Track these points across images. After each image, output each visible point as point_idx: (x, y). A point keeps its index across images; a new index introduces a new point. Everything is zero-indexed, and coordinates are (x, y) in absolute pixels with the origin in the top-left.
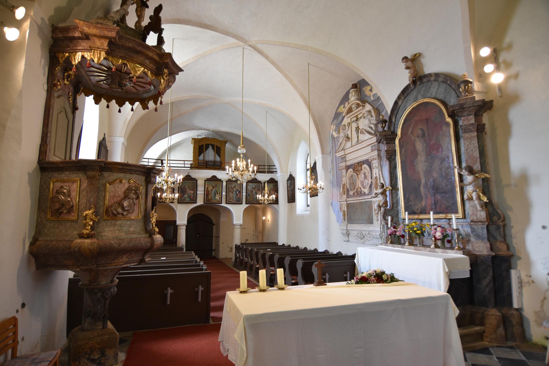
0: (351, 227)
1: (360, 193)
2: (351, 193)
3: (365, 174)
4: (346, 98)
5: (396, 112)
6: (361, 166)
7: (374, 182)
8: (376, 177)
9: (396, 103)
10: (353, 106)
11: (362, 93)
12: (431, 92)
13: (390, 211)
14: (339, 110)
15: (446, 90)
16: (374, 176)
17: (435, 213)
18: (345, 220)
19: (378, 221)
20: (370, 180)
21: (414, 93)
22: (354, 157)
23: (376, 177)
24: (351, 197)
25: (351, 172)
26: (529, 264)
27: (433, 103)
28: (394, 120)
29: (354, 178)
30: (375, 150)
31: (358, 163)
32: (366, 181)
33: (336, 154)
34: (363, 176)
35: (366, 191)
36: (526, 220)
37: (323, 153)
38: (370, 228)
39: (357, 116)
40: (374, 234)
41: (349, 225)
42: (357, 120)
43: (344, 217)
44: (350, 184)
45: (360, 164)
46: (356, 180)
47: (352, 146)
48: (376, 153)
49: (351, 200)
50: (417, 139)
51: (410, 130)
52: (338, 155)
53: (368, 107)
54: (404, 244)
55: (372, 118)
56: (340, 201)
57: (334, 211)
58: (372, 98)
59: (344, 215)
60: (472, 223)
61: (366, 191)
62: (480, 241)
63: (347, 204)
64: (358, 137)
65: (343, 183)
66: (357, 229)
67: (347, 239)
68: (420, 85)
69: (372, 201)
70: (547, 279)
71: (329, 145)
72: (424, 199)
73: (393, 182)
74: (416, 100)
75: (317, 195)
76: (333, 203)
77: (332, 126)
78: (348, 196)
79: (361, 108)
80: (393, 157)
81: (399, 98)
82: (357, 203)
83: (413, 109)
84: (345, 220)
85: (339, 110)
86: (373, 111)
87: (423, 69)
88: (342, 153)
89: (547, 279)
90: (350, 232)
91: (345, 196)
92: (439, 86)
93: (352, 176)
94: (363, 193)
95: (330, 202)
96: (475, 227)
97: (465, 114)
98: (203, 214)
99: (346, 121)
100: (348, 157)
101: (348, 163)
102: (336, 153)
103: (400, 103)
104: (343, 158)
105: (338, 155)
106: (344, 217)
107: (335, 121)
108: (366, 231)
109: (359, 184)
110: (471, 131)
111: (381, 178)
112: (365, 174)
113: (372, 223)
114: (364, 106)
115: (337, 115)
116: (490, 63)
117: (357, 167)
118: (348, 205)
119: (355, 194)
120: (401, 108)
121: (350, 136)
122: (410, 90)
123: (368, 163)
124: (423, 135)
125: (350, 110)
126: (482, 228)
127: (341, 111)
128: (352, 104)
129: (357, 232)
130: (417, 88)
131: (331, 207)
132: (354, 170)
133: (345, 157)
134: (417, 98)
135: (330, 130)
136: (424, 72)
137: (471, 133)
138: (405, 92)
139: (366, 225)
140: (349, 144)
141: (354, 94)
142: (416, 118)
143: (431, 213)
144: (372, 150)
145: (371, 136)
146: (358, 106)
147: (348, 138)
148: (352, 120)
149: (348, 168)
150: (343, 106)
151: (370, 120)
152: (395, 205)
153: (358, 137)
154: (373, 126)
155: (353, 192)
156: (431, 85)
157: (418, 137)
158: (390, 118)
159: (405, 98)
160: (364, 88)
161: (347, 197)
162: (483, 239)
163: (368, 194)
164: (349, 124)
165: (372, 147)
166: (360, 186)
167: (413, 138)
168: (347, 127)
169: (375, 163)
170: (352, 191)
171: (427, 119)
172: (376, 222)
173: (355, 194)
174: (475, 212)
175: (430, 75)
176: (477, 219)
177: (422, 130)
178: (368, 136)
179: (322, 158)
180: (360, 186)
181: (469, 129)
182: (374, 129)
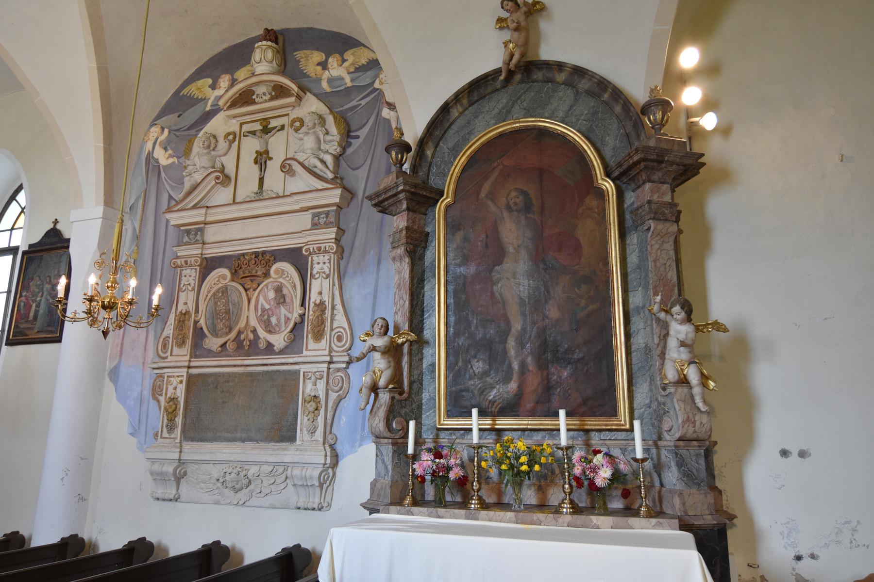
0: (194, 451)
1: (248, 346)
2: (213, 343)
3: (279, 290)
4: (236, 57)
5: (438, 133)
6: (268, 265)
7: (311, 315)
8: (322, 303)
9: (445, 109)
10: (260, 90)
11: (290, 65)
12: (552, 107)
13: (402, 401)
14: (193, 90)
15: (595, 113)
16: (314, 297)
17: (482, 414)
18: (171, 428)
19: (313, 432)
20: (298, 310)
21: (502, 99)
22: (236, 233)
23: (322, 303)
24: (210, 353)
25: (224, 277)
26: (753, 537)
27: (562, 137)
28: (429, 153)
29: (234, 297)
30: (327, 225)
31: (257, 255)
32: (283, 311)
33: (168, 216)
34: (271, 295)
35: (279, 340)
36: (747, 439)
37: (109, 201)
38: (287, 454)
39: (265, 122)
40: (297, 472)
41: (187, 446)
42: (266, 130)
43: (171, 420)
44: (214, 315)
45: (265, 259)
46: (240, 308)
47: (234, 202)
48: (331, 233)
49: (208, 366)
50: (506, 214)
51: (486, 187)
52: (175, 218)
53: (312, 105)
54: (557, 511)
55: (328, 138)
56: (154, 363)
57: (122, 399)
58: (325, 85)
59: (171, 414)
60: (681, 443)
61: (279, 340)
62: (694, 490)
63: (190, 377)
64: (261, 180)
65: (181, 308)
66: (224, 457)
67: (171, 492)
68: (522, 82)
69: (297, 372)
70: (794, 569)
71: (137, 185)
72: (515, 377)
73: (416, 321)
74: (504, 116)
75: (59, 340)
76: (123, 370)
77: (155, 130)
78: (198, 350)
79: (292, 99)
80: (419, 251)
81: (457, 97)
82: (234, 375)
83: (501, 135)
84: (171, 428)
85: (193, 90)
86: (330, 120)
87: (537, 46)
88: (196, 216)
89: (794, 569)
90: (190, 468)
91: (186, 350)
92: (576, 100)
93: (225, 290)
94: (262, 345)
95: (109, 365)
96: (683, 452)
97: (657, 176)
98: (311, 29)
99: (219, 125)
100: (212, 234)
101: (212, 251)
102: (169, 210)
103: (455, 113)
104: (193, 233)
105: (175, 218)
106: (171, 420)
107: (171, 118)
108: (261, 463)
109: (249, 317)
110: (666, 220)
111: (339, 307)
112: (279, 290)
113: (292, 439)
114: (299, 98)
115: (179, 102)
116: (681, 90)
117: (250, 267)
118: (193, 382)
119: (230, 347)
120: (455, 127)
121: (230, 170)
122: (490, 89)
123: (297, 257)
124: (527, 208)
125: (245, 98)
126: (697, 455)
127: (198, 95)
128: (257, 84)
129: (226, 468)
130: (510, 88)
131: (108, 385)
132: (234, 274)
133: (201, 230)
134: (509, 112)
135: (144, 142)
136: (538, 55)
137: (668, 224)
138: (477, 90)
139: (263, 445)
140: (223, 195)
141: (270, 55)
142: (507, 162)
143: (562, 413)
144: (315, 226)
145: (320, 184)
146: (280, 91)
147: (224, 178)
148: (246, 128)
149: (208, 265)
150: (210, 81)
151: (319, 141)
152: (415, 386)
153: (261, 180)
154: (329, 159)
155: (222, 341)
156: (554, 91)
157: (509, 208)
158: (422, 143)
159: (471, 104)
160: (300, 54)
161: (194, 355)
162: (699, 485)
163: (282, 352)
164: (232, 138)
165: (315, 215)
166: (253, 322)
167: (493, 208)
168: (223, 145)
169: (321, 264)
170: (215, 333)
171: (541, 171)
172: (306, 437)
173: (230, 347)
174: (691, 416)
175: (560, 66)
176: (695, 432)
177: (525, 194)
178: (302, 181)
179: (104, 218)
180: (253, 322)
181: (664, 214)
182: (331, 166)
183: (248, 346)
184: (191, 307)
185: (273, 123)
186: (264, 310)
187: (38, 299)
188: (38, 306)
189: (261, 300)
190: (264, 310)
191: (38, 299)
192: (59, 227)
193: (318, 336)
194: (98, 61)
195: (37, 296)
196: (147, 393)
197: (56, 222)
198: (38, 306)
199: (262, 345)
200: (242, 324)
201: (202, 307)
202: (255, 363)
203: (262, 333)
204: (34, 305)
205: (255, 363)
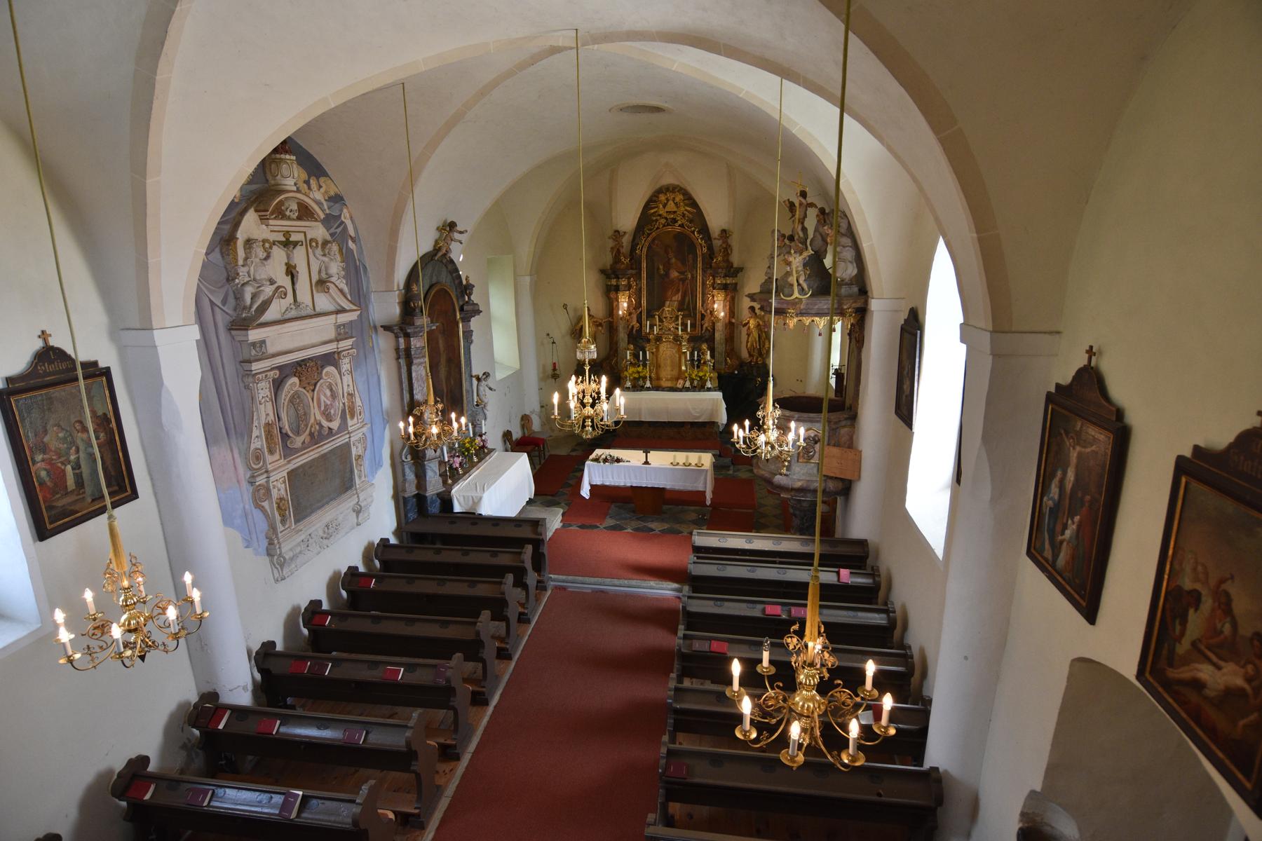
25: (293, 384)
35: (335, 425)
39: (287, 234)
75: (137, 497)
78: (288, 452)
109: (316, 414)
166: (319, 417)
180: (319, 417)
183: (317, 437)
184: (271, 418)
185: (293, 238)
186: (326, 406)
187: (72, 458)
188: (77, 466)
189: (323, 398)
190: (326, 406)
191: (72, 458)
192: (53, 342)
193: (352, 417)
194: (154, 70)
195: (68, 454)
196: (249, 505)
197: (44, 335)
198: (77, 466)
199: (326, 432)
200: (312, 420)
201: (284, 416)
202: (327, 447)
203: (325, 423)
204: (69, 468)
205: (327, 447)
